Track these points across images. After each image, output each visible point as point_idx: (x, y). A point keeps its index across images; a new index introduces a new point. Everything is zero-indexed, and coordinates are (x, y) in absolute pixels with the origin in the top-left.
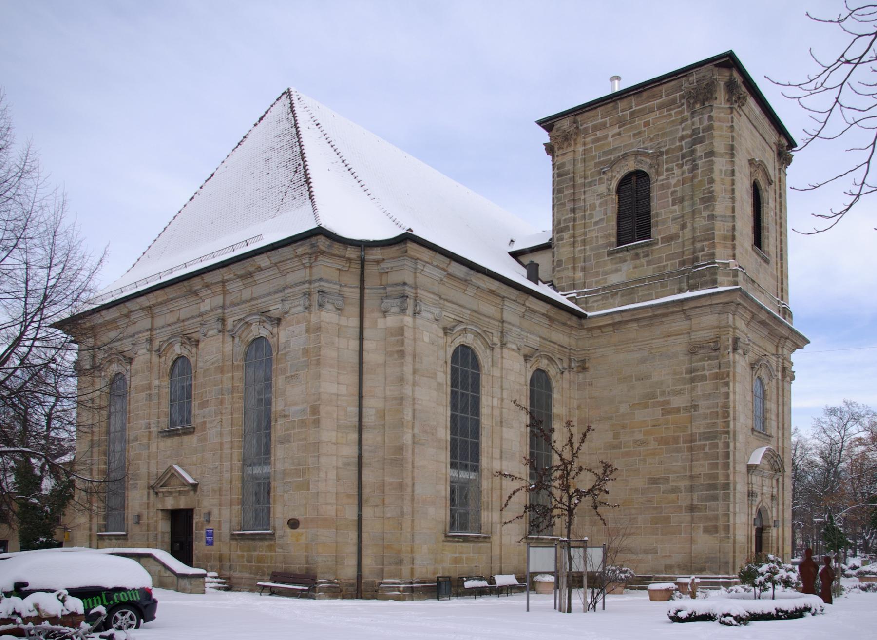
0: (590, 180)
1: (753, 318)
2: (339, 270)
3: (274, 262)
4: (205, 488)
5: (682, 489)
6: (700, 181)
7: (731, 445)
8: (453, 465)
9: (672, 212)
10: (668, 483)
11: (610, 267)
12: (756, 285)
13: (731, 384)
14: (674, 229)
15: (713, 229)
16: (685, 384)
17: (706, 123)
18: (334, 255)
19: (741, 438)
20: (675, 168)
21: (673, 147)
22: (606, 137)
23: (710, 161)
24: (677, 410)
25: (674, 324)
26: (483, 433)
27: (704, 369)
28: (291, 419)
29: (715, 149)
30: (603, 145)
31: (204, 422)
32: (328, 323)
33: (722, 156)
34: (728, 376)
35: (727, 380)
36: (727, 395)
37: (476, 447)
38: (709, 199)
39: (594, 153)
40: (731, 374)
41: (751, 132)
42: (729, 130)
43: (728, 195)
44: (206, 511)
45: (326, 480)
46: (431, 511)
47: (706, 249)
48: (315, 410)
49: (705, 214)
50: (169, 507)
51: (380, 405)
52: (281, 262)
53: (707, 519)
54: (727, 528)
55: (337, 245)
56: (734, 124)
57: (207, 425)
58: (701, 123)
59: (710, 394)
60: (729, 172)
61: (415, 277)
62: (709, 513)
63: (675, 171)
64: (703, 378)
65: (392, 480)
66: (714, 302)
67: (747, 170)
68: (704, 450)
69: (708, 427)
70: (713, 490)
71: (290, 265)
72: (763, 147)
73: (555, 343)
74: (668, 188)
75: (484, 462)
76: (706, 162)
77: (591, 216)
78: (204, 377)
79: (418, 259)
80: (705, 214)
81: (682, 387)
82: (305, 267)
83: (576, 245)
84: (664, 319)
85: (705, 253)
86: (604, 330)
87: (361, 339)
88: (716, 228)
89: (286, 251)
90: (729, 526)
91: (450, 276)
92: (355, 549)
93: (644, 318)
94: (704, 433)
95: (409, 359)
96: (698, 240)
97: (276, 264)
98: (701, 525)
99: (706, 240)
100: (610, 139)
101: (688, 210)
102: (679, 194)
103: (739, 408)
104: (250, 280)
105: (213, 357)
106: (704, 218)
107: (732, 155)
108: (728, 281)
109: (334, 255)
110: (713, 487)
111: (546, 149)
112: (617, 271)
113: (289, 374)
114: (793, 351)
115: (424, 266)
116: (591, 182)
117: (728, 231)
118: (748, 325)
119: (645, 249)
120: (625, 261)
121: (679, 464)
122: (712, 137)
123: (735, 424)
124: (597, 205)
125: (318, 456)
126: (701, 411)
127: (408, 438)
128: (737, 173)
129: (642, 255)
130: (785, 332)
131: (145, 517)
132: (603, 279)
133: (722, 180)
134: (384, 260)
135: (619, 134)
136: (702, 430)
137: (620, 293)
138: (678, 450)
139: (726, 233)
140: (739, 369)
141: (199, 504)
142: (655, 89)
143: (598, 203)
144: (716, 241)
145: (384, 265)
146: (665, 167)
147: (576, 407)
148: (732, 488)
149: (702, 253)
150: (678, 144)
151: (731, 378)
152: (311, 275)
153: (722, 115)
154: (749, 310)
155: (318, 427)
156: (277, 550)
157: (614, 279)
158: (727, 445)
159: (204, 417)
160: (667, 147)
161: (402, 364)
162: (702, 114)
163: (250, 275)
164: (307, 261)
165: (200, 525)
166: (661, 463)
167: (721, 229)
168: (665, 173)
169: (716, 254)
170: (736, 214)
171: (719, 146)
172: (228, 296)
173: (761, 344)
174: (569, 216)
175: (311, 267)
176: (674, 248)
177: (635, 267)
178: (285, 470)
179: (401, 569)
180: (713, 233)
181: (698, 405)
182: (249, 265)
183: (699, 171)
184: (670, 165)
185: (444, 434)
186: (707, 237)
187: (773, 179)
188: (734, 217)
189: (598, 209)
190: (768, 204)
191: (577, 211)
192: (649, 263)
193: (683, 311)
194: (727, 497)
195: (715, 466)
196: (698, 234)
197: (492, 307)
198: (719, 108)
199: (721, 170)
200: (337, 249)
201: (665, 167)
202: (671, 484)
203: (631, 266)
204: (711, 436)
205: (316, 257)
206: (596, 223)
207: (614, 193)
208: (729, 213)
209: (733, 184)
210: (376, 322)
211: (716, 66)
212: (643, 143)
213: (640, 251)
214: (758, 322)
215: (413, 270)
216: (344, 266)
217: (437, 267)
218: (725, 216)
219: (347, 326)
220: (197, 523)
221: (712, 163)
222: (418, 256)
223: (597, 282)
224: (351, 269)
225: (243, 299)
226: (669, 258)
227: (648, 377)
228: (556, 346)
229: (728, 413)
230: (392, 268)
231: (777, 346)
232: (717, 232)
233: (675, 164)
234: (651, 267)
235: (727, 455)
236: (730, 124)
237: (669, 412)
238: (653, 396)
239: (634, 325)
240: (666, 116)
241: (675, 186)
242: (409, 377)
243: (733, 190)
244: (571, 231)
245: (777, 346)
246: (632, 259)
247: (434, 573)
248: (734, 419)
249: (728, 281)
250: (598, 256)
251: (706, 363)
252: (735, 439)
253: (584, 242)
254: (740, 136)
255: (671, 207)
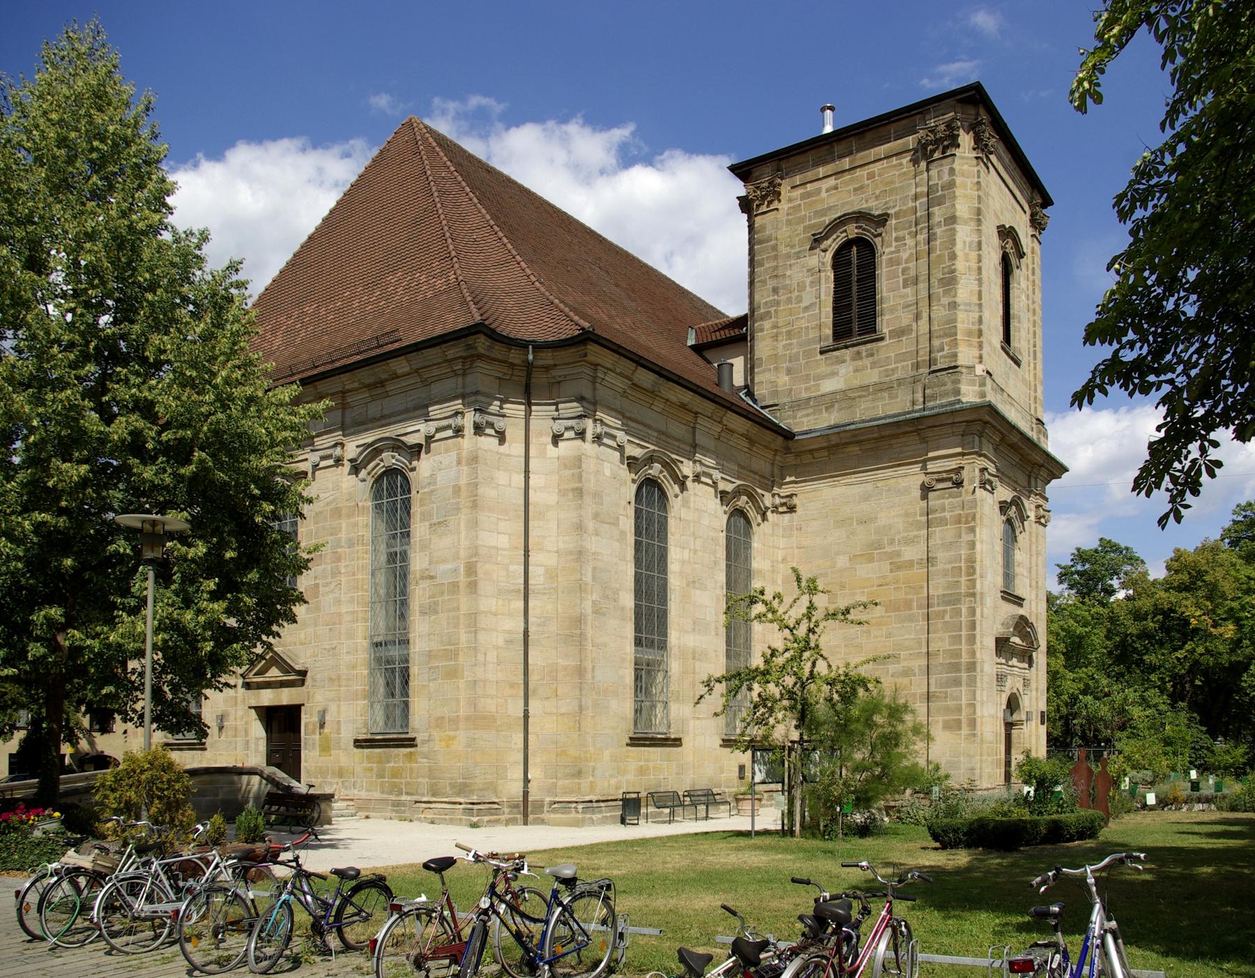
0: (797, 249)
1: (1002, 439)
2: (499, 378)
3: (415, 367)
4: (318, 676)
5: (917, 671)
6: (939, 256)
7: (978, 611)
8: (638, 642)
9: (902, 297)
10: (898, 662)
11: (823, 369)
12: (1005, 395)
13: (978, 530)
14: (906, 319)
15: (955, 320)
16: (919, 529)
17: (946, 177)
18: (494, 360)
19: (989, 601)
20: (907, 237)
21: (904, 208)
22: (819, 191)
23: (951, 229)
24: (910, 564)
25: (905, 449)
26: (673, 597)
27: (944, 510)
28: (438, 581)
29: (958, 214)
30: (815, 201)
31: (317, 586)
32: (486, 451)
33: (966, 223)
34: (974, 519)
35: (972, 524)
36: (972, 545)
37: (663, 615)
38: (950, 281)
39: (803, 213)
40: (978, 516)
41: (1000, 189)
42: (975, 188)
43: (974, 276)
44: (320, 708)
45: (485, 665)
46: (614, 704)
47: (946, 348)
48: (471, 569)
49: (945, 301)
50: (266, 703)
51: (552, 561)
52: (425, 367)
53: (948, 710)
54: (972, 723)
55: (498, 346)
56: (981, 180)
57: (321, 589)
58: (940, 177)
59: (951, 543)
60: (975, 244)
61: (595, 389)
62: (950, 703)
63: (907, 241)
64: (943, 522)
65: (566, 663)
66: (956, 420)
67: (995, 240)
68: (943, 618)
69: (948, 588)
70: (955, 672)
71: (436, 372)
72: (1013, 207)
73: (755, 473)
74: (898, 264)
75: (674, 637)
76: (946, 231)
77: (799, 299)
78: (316, 523)
79: (598, 365)
80: (945, 301)
81: (916, 533)
82: (456, 375)
83: (780, 338)
84: (893, 441)
85: (945, 353)
86: (816, 455)
87: (527, 472)
88: (959, 320)
89: (432, 354)
90: (975, 719)
91: (635, 386)
92: (521, 757)
93: (869, 440)
94: (944, 595)
95: (588, 500)
96: (935, 335)
97: (416, 371)
98: (941, 719)
99: (946, 335)
100: (824, 194)
101: (924, 293)
102: (912, 273)
103: (987, 562)
104: (380, 391)
105: (328, 494)
106: (944, 306)
107: (979, 222)
108: (973, 391)
109: (494, 360)
110: (955, 667)
111: (740, 205)
112: (834, 374)
113: (435, 521)
114: (1049, 482)
115: (605, 374)
116: (800, 252)
117: (973, 323)
118: (995, 449)
119: (869, 346)
120: (844, 361)
121: (912, 637)
122: (954, 197)
123: (982, 583)
124: (808, 284)
125: (476, 632)
126: (940, 566)
127: (588, 607)
128: (984, 246)
129: (864, 354)
130: (1038, 458)
131: (232, 717)
132: (814, 385)
133: (967, 254)
134: (555, 365)
135: (836, 188)
136: (941, 592)
137: (836, 406)
138: (911, 619)
139: (971, 326)
140: (986, 510)
141: (308, 699)
142: (882, 128)
143: (808, 281)
144: (958, 337)
145: (556, 373)
146: (894, 235)
147: (780, 559)
148: (978, 669)
149: (941, 354)
150: (911, 204)
151: (978, 522)
152: (464, 386)
153: (965, 167)
154: (998, 431)
155: (476, 593)
156: (420, 760)
157: (828, 386)
158: (972, 611)
159: (316, 578)
160: (897, 209)
161: (580, 507)
162: (942, 165)
163: (382, 383)
164: (460, 367)
165: (311, 727)
166: (889, 635)
167: (964, 320)
168: (894, 244)
169: (959, 355)
170: (983, 301)
171: (963, 209)
172: (348, 412)
173: (1011, 475)
174: (771, 298)
175: (464, 375)
176: (907, 344)
177: (856, 371)
178: (430, 651)
179: (579, 784)
180: (955, 327)
181: (936, 558)
182: (380, 371)
183: (938, 242)
184: (901, 234)
185: (628, 600)
186: (947, 331)
187: (1025, 251)
188: (980, 305)
189: (808, 288)
190: (1019, 284)
191: (781, 292)
192: (874, 365)
193: (918, 431)
194: (972, 682)
195: (957, 639)
196: (937, 328)
197: (683, 426)
198: (962, 158)
199: (965, 242)
200: (499, 351)
201: (894, 235)
202: (902, 665)
203: (851, 369)
204: (953, 600)
205: (472, 362)
206: (806, 309)
207: (829, 268)
208: (975, 300)
209: (980, 261)
210: (545, 449)
211: (959, 101)
212: (867, 201)
213: (862, 348)
214: (1009, 445)
215: (590, 379)
216: (505, 374)
217: (621, 374)
218: (969, 304)
219: (509, 455)
220: (306, 725)
221: (953, 233)
222: (599, 361)
223: (807, 389)
224: (513, 378)
225: (369, 416)
226: (900, 358)
227: (873, 520)
228: (757, 477)
229: (973, 568)
230: (565, 376)
231: (1029, 476)
232: (959, 326)
233: (906, 232)
234: (876, 370)
235: (973, 626)
236: (976, 180)
237: (896, 567)
238: (880, 546)
239: (855, 449)
240: (895, 166)
241: (907, 261)
242: (590, 525)
243: (980, 269)
244: (773, 319)
245: (1029, 476)
246: (853, 359)
247: (617, 788)
248: (981, 577)
249: (973, 391)
250: (808, 354)
251: (947, 502)
252: (982, 604)
253: (789, 334)
254: (987, 195)
255: (902, 290)
